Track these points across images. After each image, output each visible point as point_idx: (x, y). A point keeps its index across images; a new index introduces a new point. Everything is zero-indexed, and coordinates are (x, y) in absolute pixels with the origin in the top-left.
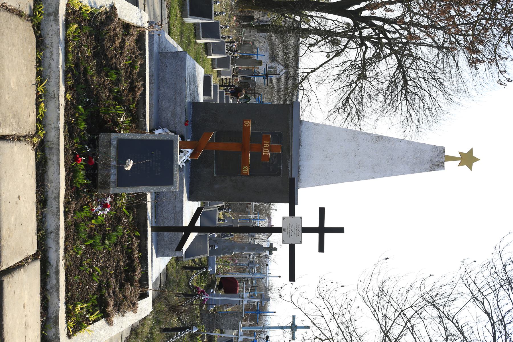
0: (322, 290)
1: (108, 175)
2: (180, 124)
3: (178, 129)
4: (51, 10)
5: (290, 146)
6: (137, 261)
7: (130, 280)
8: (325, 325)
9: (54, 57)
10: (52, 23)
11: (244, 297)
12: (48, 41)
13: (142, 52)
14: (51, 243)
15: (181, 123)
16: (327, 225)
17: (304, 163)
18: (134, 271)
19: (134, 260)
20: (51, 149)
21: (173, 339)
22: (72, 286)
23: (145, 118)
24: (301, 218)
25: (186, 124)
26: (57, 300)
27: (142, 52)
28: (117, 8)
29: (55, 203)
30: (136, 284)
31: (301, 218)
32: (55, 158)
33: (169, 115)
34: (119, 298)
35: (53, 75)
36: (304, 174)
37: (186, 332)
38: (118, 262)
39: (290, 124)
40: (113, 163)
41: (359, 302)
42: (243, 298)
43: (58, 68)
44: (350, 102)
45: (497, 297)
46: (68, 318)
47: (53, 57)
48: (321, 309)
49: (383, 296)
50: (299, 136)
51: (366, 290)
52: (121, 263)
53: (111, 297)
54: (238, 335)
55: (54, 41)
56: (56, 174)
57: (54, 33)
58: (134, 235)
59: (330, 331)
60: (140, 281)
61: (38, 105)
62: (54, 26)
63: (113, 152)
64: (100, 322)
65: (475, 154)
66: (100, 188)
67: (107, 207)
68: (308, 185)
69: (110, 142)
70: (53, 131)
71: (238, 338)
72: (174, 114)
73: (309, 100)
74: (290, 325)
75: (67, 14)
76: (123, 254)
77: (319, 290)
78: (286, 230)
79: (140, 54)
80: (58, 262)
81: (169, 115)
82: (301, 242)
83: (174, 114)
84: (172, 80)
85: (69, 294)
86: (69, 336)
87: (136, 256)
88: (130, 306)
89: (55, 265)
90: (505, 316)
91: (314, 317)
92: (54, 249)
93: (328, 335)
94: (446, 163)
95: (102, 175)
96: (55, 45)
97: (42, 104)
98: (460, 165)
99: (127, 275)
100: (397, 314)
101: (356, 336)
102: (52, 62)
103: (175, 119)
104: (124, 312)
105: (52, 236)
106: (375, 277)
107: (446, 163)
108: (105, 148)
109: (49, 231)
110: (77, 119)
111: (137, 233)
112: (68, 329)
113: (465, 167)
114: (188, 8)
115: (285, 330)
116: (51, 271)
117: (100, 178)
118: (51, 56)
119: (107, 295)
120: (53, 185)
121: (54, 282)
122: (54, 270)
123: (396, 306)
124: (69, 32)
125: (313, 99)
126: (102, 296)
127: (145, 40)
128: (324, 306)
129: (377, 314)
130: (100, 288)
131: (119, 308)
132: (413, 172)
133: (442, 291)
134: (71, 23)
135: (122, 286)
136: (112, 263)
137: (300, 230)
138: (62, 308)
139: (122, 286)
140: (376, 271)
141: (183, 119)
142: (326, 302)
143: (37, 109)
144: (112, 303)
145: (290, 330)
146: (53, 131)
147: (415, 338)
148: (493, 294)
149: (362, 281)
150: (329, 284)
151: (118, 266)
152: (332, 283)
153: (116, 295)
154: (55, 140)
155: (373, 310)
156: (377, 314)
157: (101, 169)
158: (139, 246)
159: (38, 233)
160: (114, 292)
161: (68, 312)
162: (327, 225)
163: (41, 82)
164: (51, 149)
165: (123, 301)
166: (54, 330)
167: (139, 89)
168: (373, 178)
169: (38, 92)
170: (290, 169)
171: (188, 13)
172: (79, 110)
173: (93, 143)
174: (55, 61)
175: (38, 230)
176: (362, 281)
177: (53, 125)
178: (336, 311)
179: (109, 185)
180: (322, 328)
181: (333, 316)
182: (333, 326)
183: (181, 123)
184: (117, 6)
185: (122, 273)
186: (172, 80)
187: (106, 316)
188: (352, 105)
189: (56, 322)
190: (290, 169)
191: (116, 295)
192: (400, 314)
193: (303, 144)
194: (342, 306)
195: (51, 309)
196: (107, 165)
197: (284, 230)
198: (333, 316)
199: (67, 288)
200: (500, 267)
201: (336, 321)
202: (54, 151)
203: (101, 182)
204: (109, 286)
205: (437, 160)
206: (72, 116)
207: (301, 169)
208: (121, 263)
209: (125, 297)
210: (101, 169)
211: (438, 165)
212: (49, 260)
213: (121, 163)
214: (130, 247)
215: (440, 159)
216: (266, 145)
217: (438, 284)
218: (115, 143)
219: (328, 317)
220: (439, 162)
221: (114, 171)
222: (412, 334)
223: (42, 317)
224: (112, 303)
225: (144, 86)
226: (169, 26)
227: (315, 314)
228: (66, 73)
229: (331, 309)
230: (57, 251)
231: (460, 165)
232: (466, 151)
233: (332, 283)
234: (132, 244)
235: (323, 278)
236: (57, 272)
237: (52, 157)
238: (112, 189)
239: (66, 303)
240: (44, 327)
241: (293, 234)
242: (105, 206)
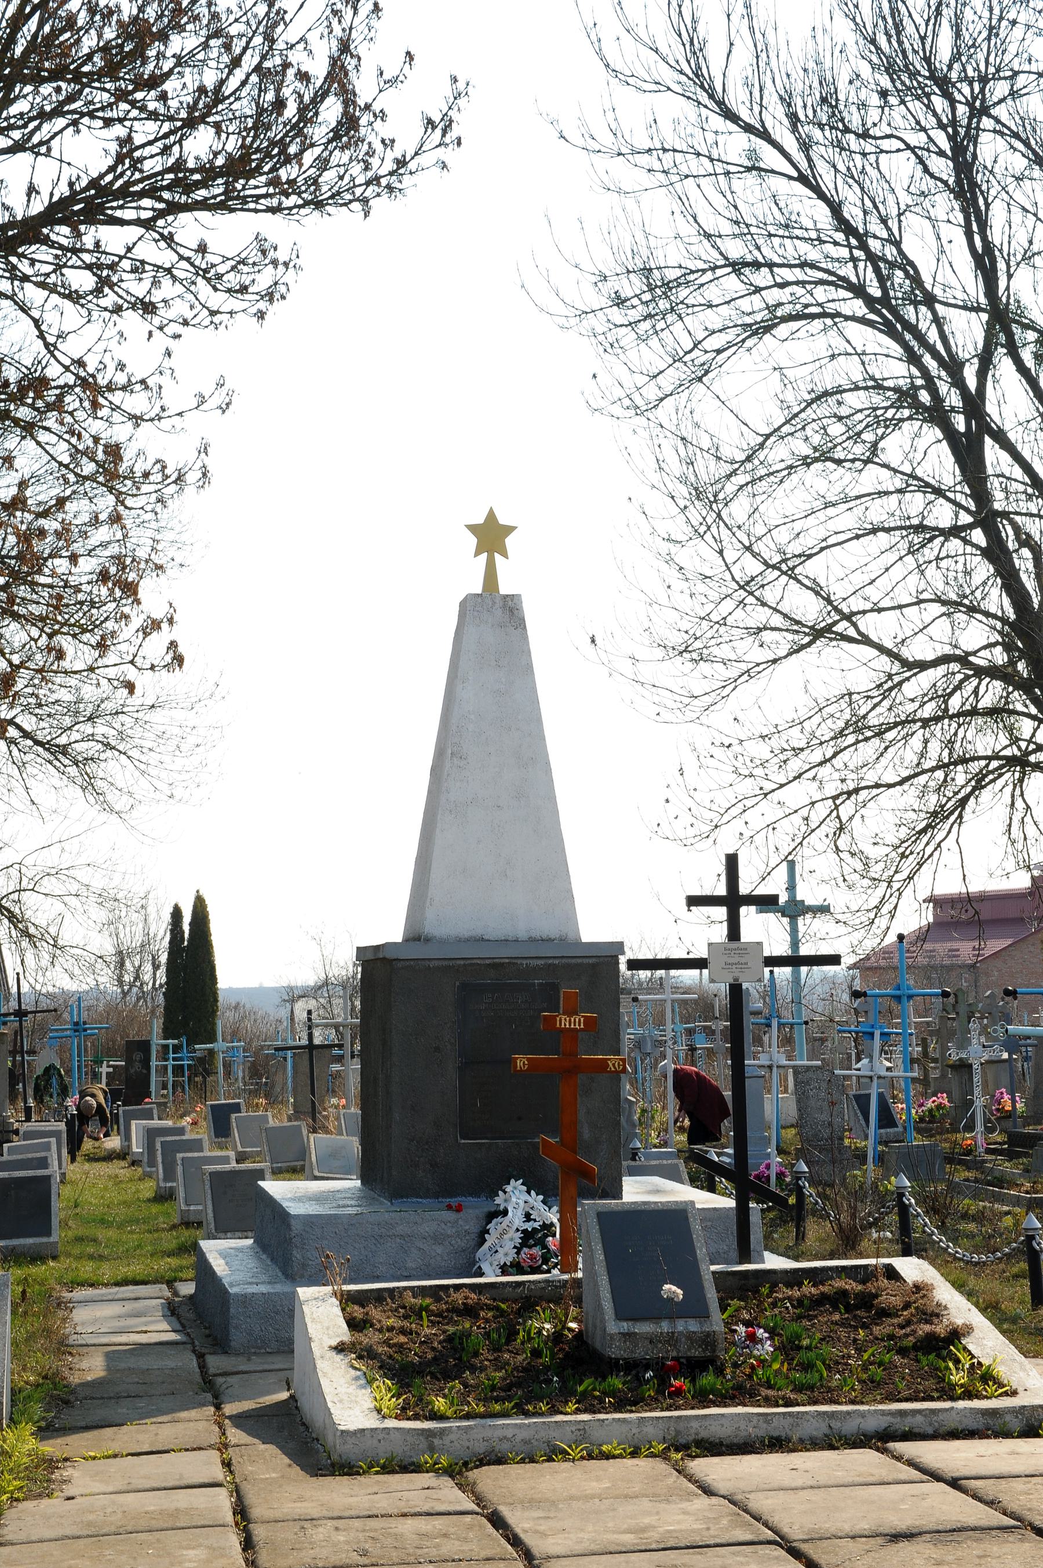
0: (692, 832)
1: (690, 1336)
2: (461, 1222)
3: (474, 1228)
4: (423, 1445)
5: (488, 962)
6: (824, 1289)
7: (866, 1301)
8: (797, 819)
9: (509, 1433)
10: (447, 1440)
11: (768, 1063)
12: (481, 1448)
13: (386, 1295)
14: (850, 1427)
15: (457, 1222)
16: (721, 890)
17: (522, 929)
18: (844, 1293)
19: (822, 1293)
20: (678, 1432)
21: (933, 1233)
22: (918, 1391)
23: (523, 1283)
24: (710, 945)
25: (459, 1209)
26: (953, 1413)
27: (386, 1295)
28: (338, 1340)
29: (776, 1422)
30: (871, 1287)
31: (710, 945)
32: (695, 1424)
33: (439, 1251)
34: (912, 1315)
35: (543, 1434)
36: (546, 927)
37: (910, 1205)
38: (836, 1323)
39: (437, 963)
40: (665, 1326)
41: (720, 718)
42: (770, 1067)
43: (529, 1425)
44: (63, 740)
45: (696, 309)
46: (979, 1396)
47: (510, 1436)
48: (747, 834)
49: (698, 644)
50: (460, 941)
51: (687, 700)
52: (837, 1317)
53: (914, 1332)
54: (871, 1078)
55: (480, 1436)
56: (723, 1421)
57: (465, 1436)
58: (769, 1296)
59: (813, 803)
60: (863, 1282)
61: (608, 1456)
62: (452, 1437)
63: (644, 1328)
64: (970, 1347)
65: (480, 519)
66: (714, 1351)
67: (754, 1334)
68: (571, 916)
69: (627, 1336)
70: (645, 1429)
71: (879, 1077)
72: (437, 1239)
73: (53, 871)
74: (785, 920)
75: (416, 1417)
76: (816, 1317)
77: (693, 841)
78: (736, 975)
79: (392, 1298)
80: (883, 1413)
81: (439, 1250)
82: (760, 944)
83: (437, 1239)
84: (357, 1246)
85: (936, 1395)
86: (1014, 1393)
87: (813, 1290)
88: (924, 1296)
89: (889, 1418)
90: (751, 285)
91: (772, 849)
92: (861, 1420)
93: (822, 809)
94: (504, 590)
95: (689, 1349)
96: (488, 1433)
97: (604, 1448)
98: (505, 555)
99: (857, 1307)
100: (750, 600)
101: (817, 719)
102: (518, 1438)
103: (449, 1236)
104: (939, 1305)
105: (836, 1425)
106: (646, 672)
107: (504, 590)
108: (636, 1345)
109: (827, 1431)
110: (605, 1394)
111: (765, 1290)
112: (1001, 1395)
113: (510, 541)
114: (30, 1241)
115: (800, 935)
116: (905, 1425)
117: (696, 1353)
118: (508, 1440)
119: (911, 1338)
120: (743, 1427)
121: (919, 1418)
122: (899, 1419)
123: (728, 605)
124: (449, 1413)
125: (50, 858)
126: (915, 1347)
127: (357, 1291)
128: (738, 825)
129: (758, 665)
130: (902, 1352)
131: (933, 1314)
132: (529, 669)
133: (675, 467)
134: (432, 1410)
135: (885, 1313)
136: (842, 1333)
137: (734, 945)
138: (961, 1404)
139: (885, 1313)
140: (626, 667)
141: (450, 1216)
142: (726, 818)
143: (614, 1457)
144: (927, 1328)
145: (800, 921)
146: (645, 1429)
147: (822, 549)
148: (686, 319)
149: (658, 709)
150: (672, 809)
151: (842, 1324)
152: (667, 801)
153: (909, 1323)
154: (661, 1425)
155: (745, 677)
156: (758, 665)
157: (679, 1351)
158: (789, 1285)
159: (837, 1448)
160: (902, 1327)
161: (969, 1394)
162: (721, 890)
163: (564, 1452)
164: (678, 1432)
165: (917, 1308)
166: (1008, 1418)
167: (466, 1298)
168: (548, 763)
169: (582, 1458)
170: (542, 962)
171: (44, 1240)
172: (585, 1390)
173: (632, 1367)
174: (517, 1431)
175: (832, 1447)
176: (658, 709)
177: (634, 1431)
178: (748, 787)
179: (708, 1334)
180: (804, 828)
181: (766, 795)
182: (798, 794)
183: (457, 1222)
184: (334, 1343)
185: (855, 1316)
186: (357, 1246)
187: (956, 1335)
188: (75, 736)
189: (994, 1413)
190: (542, 962)
191: (909, 1323)
192: (751, 593)
193: (479, 932)
194: (736, 771)
195: (972, 1424)
196: (671, 1339)
197: (736, 980)
198: (766, 795)
199: (924, 1399)
200: (617, 315)
201: (782, 786)
202: (681, 1426)
203: (704, 1351)
204: (891, 1337)
205: (499, 612)
206: (601, 1401)
207: (536, 934)
208: (837, 1317)
209: (907, 1306)
210: (679, 1351)
211: (511, 610)
212: (880, 1430)
213: (671, 1310)
214: (800, 1303)
215: (497, 606)
216: (564, 1022)
217: (655, 478)
218: (625, 1324)
219: (769, 810)
220: (504, 606)
221: (681, 1326)
222: (810, 556)
223: (988, 1437)
224: (927, 1328)
225: (457, 1287)
226: (117, 1284)
227: (764, 851)
228: (527, 1414)
229: (748, 803)
230: (863, 1415)
231: (505, 555)
232: (473, 541)
233: (667, 801)
234: (790, 1298)
235: (656, 828)
236: (902, 1413)
237: (693, 1431)
238: (716, 1328)
239: (953, 1399)
240: (1005, 1434)
241: (743, 961)
242: (752, 1337)
